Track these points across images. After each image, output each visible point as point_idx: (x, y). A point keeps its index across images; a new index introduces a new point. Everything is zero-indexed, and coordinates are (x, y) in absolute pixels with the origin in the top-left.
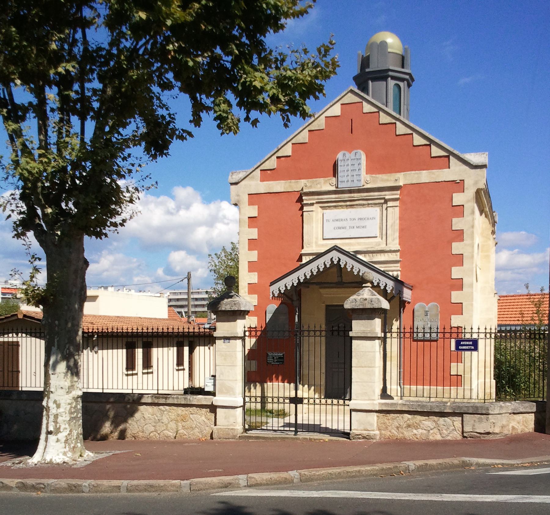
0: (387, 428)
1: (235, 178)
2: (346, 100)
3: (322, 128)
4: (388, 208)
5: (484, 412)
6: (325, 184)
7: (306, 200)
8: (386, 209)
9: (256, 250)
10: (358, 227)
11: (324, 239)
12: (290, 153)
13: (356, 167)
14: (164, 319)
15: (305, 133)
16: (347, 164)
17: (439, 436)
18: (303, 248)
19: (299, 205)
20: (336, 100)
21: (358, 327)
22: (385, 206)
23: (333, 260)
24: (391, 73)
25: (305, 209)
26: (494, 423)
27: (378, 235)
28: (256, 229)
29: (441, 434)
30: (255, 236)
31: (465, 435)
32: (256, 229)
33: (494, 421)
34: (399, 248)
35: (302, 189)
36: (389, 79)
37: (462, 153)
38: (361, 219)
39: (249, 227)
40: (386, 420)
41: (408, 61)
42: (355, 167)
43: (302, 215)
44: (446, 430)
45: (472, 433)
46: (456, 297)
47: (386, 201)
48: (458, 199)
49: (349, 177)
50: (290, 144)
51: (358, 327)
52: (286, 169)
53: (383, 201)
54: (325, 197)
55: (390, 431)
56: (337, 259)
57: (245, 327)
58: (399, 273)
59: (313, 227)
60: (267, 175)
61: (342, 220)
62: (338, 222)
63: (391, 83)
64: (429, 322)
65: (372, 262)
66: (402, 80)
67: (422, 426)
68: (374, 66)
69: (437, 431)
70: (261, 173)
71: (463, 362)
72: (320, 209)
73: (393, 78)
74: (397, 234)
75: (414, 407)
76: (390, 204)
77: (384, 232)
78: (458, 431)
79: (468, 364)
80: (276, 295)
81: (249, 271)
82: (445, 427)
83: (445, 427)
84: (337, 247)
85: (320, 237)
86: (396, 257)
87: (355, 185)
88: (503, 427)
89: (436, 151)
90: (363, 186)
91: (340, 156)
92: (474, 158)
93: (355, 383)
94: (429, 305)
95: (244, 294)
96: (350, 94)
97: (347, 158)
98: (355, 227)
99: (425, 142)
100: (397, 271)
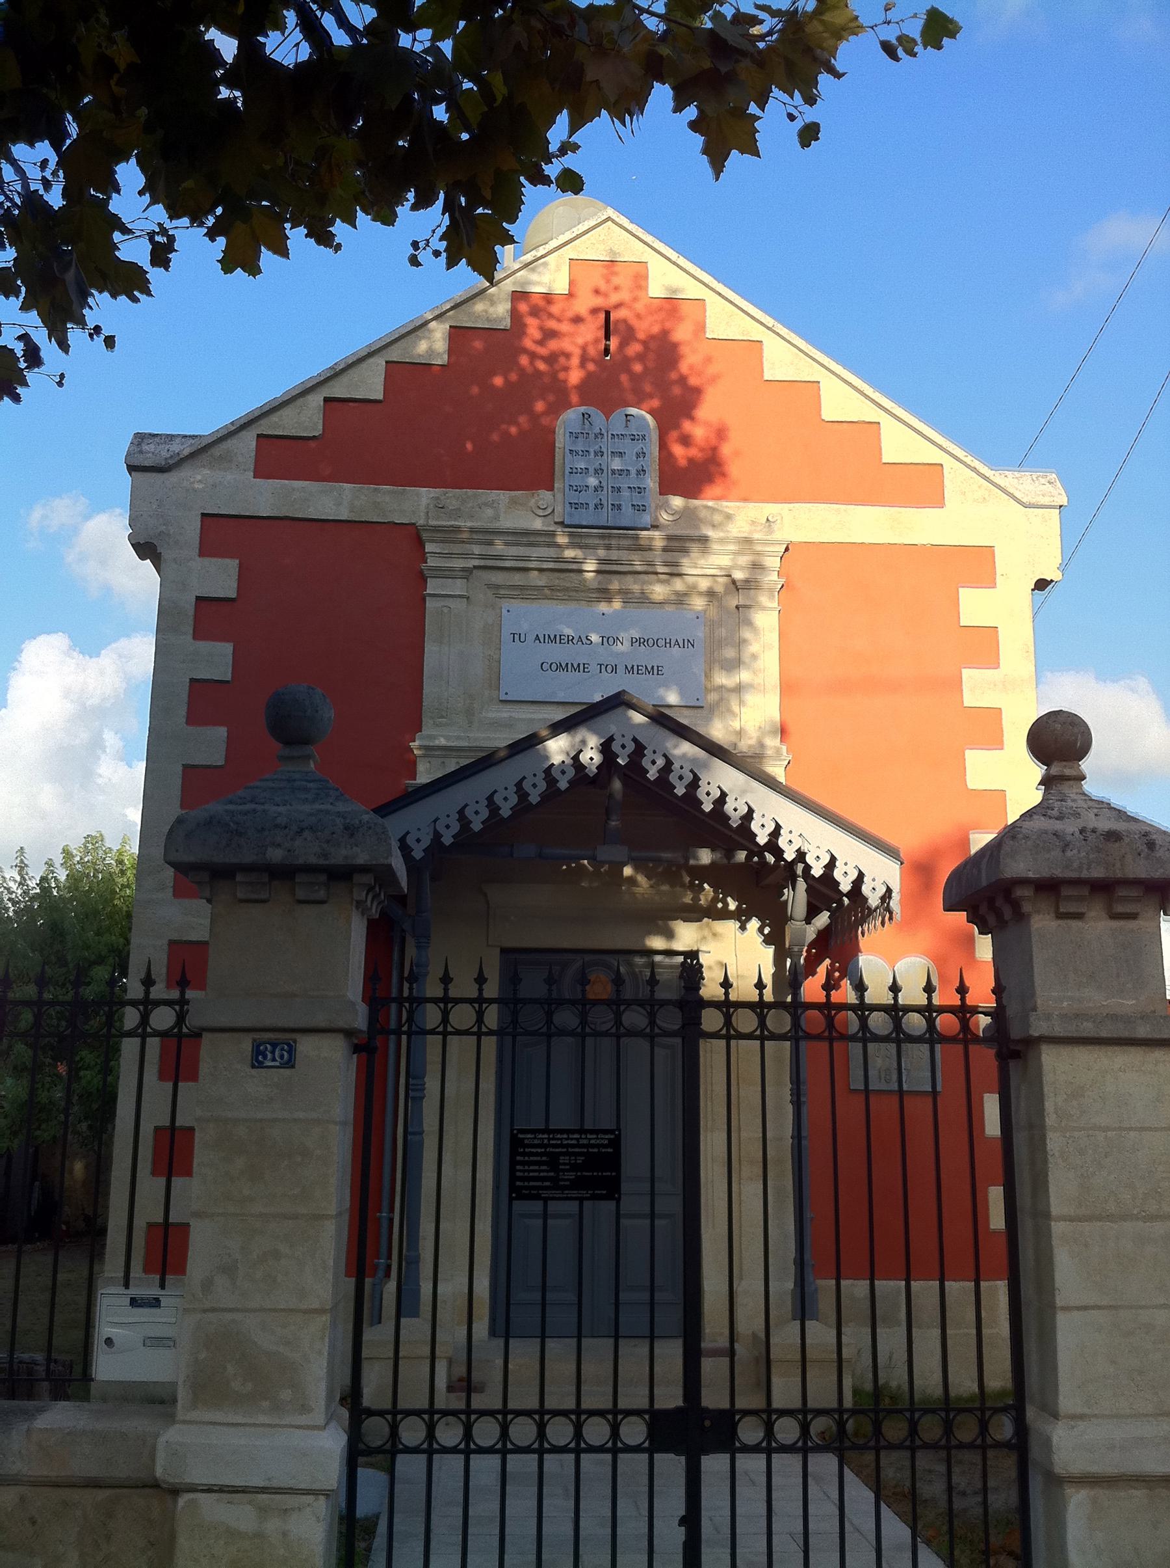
14: (216, 767)
48: (975, 607)
49: (603, 495)
50: (379, 363)
98: (621, 669)
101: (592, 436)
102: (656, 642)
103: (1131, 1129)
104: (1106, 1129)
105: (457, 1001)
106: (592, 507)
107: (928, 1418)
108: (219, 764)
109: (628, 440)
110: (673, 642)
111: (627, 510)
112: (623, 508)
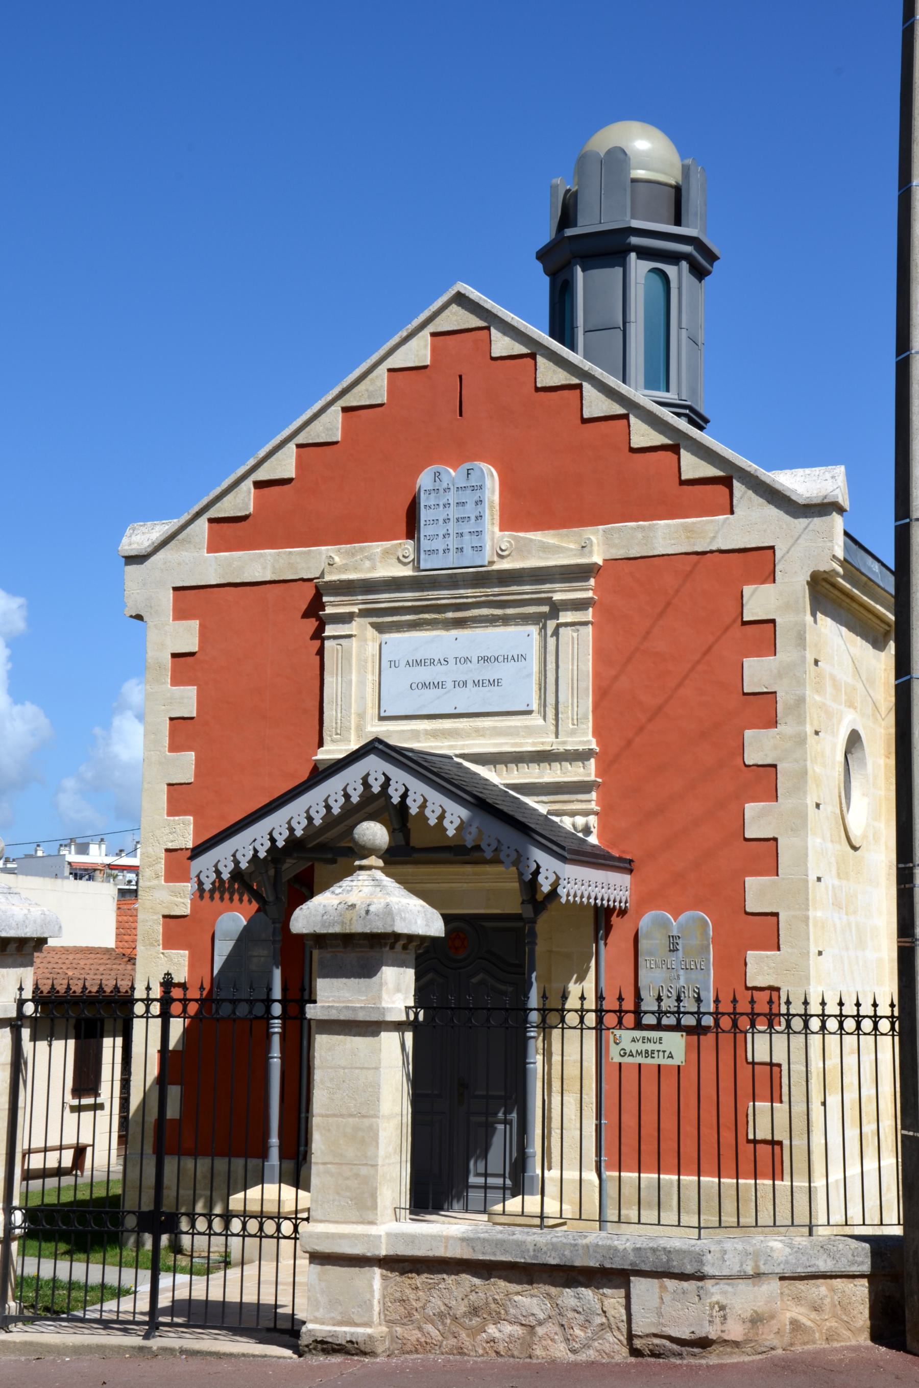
0: (410, 1315)
1: (139, 538)
2: (444, 323)
3: (379, 402)
4: (562, 630)
5: (689, 1269)
6: (384, 559)
7: (333, 604)
8: (556, 633)
9: (189, 749)
10: (476, 684)
11: (381, 719)
12: (289, 471)
13: (470, 510)
15: (335, 416)
16: (445, 501)
17: (562, 1346)
18: (321, 744)
19: (312, 624)
20: (416, 322)
21: (332, 996)
22: (551, 625)
23: (371, 780)
24: (634, 240)
25: (329, 630)
26: (722, 1308)
27: (535, 707)
28: (194, 689)
29: (567, 1340)
30: (190, 710)
31: (638, 1343)
32: (194, 689)
33: (724, 1301)
34: (594, 746)
35: (322, 575)
36: (633, 255)
37: (769, 471)
38: (486, 659)
39: (175, 682)
40: (408, 1291)
41: (694, 201)
42: (471, 512)
43: (321, 652)
44: (583, 1327)
45: (657, 1341)
46: (758, 893)
47: (556, 608)
48: (758, 601)
50: (292, 447)
51: (332, 996)
52: (282, 513)
53: (545, 609)
54: (385, 599)
55: (420, 1329)
56: (382, 779)
57: (21, 989)
58: (593, 820)
59: (351, 681)
60: (229, 531)
61: (432, 662)
62: (420, 669)
63: (639, 268)
64: (682, 972)
65: (514, 787)
66: (674, 258)
67: (512, 1311)
68: (586, 224)
69: (557, 1329)
70: (210, 529)
71: (785, 1098)
72: (371, 632)
73: (645, 254)
74: (588, 703)
75: (488, 1249)
76: (566, 617)
77: (551, 700)
78: (616, 1333)
79: (799, 1108)
80: (208, 886)
81: (170, 814)
82: (580, 1318)
83: (580, 1318)
84: (380, 741)
85: (372, 712)
86: (588, 772)
87: (469, 560)
88: (756, 1320)
89: (692, 466)
90: (491, 563)
91: (425, 480)
92: (800, 483)
93: (321, 1167)
94: (683, 917)
95: (155, 882)
96: (454, 308)
97: (445, 485)
99: (659, 439)
100: (586, 813)
101: (442, 491)
102: (496, 659)
103: (356, 1068)
104: (344, 1068)
105: (190, 1000)
106: (441, 552)
107: (287, 1234)
108: (190, 781)
109: (469, 491)
110: (510, 658)
111: (468, 551)
112: (464, 550)
